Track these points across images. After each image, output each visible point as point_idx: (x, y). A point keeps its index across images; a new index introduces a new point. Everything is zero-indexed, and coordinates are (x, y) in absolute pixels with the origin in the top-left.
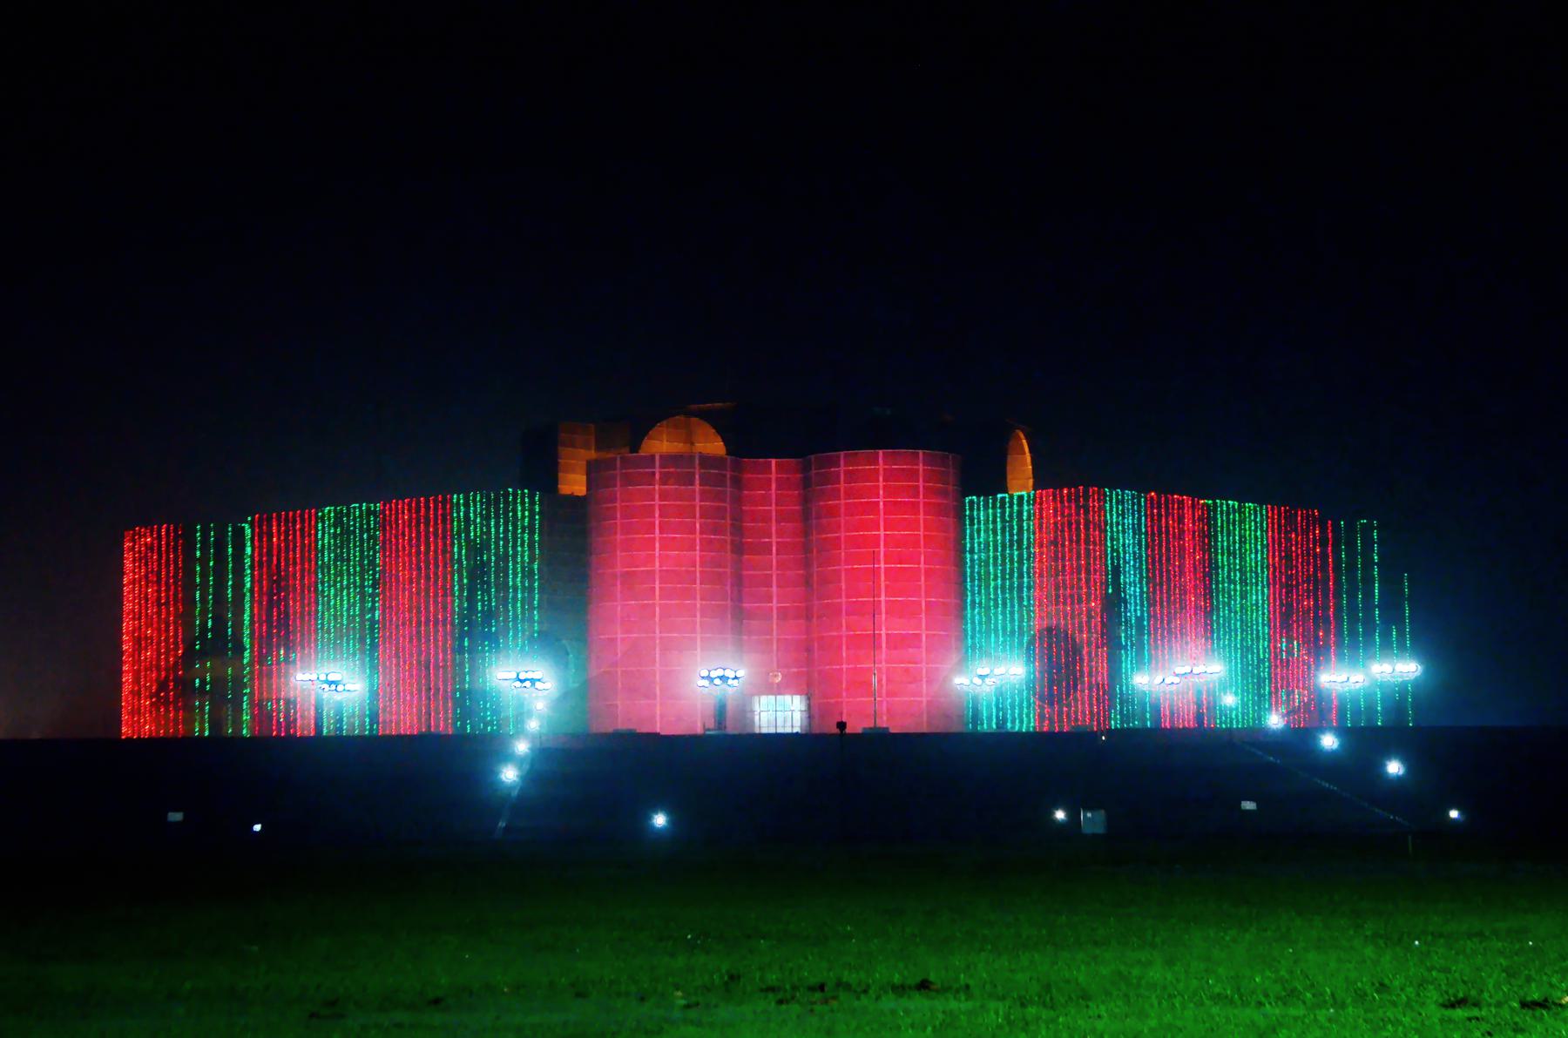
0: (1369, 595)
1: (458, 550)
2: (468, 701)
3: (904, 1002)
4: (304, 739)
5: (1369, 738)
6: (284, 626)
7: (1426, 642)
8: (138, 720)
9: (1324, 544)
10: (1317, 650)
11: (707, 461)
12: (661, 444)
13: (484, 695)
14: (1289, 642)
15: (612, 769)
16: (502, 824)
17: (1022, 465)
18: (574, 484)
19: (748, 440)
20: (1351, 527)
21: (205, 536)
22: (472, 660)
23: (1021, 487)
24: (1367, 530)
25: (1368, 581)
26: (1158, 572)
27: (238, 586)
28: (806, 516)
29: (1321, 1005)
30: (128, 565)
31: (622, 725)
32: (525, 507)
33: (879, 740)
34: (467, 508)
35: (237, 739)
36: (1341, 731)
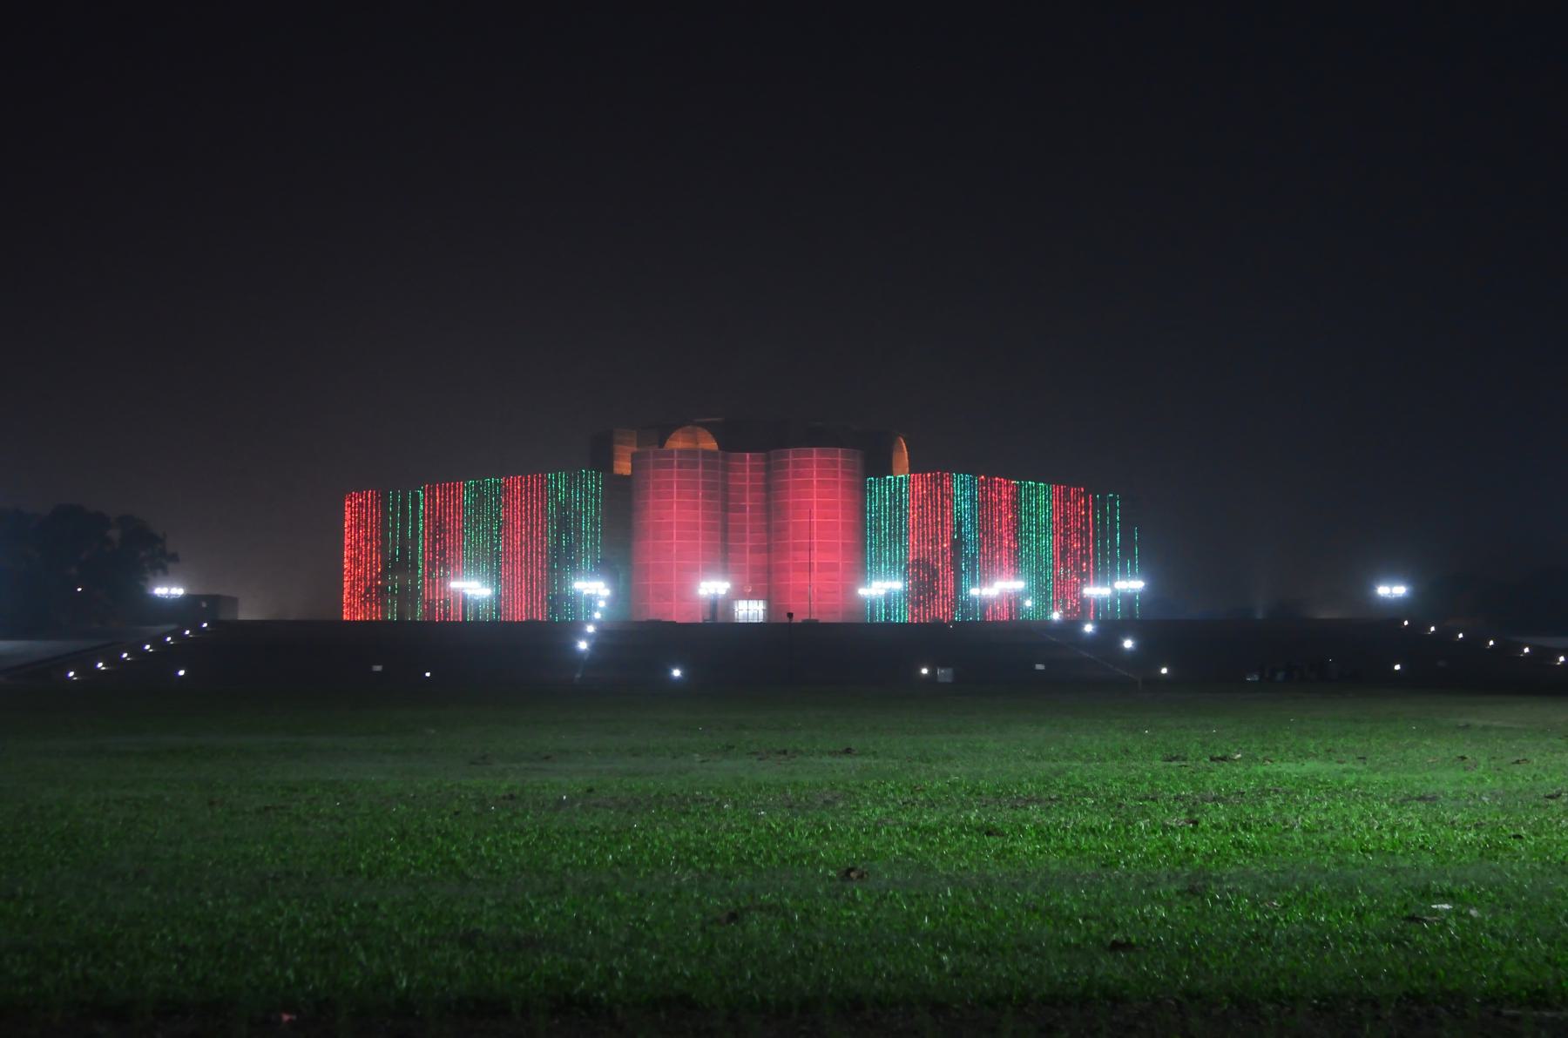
0: (1113, 540)
1: (551, 508)
2: (559, 600)
3: (837, 760)
4: (456, 623)
5: (1112, 627)
6: (442, 559)
7: (1146, 570)
8: (352, 610)
9: (1087, 509)
10: (1084, 578)
11: (706, 453)
12: (677, 443)
13: (568, 599)
14: (1066, 568)
15: (643, 644)
16: (578, 676)
17: (902, 457)
18: (623, 467)
19: (733, 439)
20: (1103, 499)
21: (395, 498)
22: (560, 578)
23: (902, 474)
24: (1113, 500)
25: (1113, 531)
26: (986, 530)
27: (415, 528)
28: (768, 488)
29: (1091, 760)
30: (347, 515)
31: (652, 617)
32: (592, 482)
33: (811, 626)
34: (558, 482)
35: (414, 622)
36: (1096, 621)
